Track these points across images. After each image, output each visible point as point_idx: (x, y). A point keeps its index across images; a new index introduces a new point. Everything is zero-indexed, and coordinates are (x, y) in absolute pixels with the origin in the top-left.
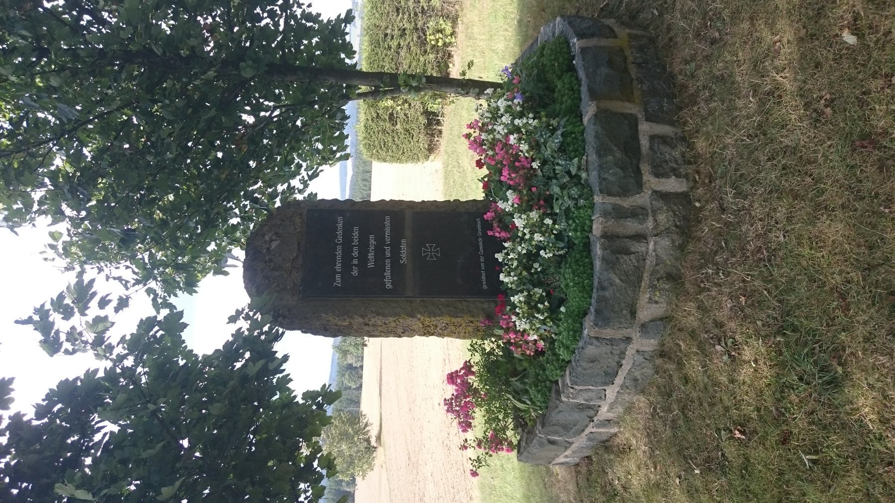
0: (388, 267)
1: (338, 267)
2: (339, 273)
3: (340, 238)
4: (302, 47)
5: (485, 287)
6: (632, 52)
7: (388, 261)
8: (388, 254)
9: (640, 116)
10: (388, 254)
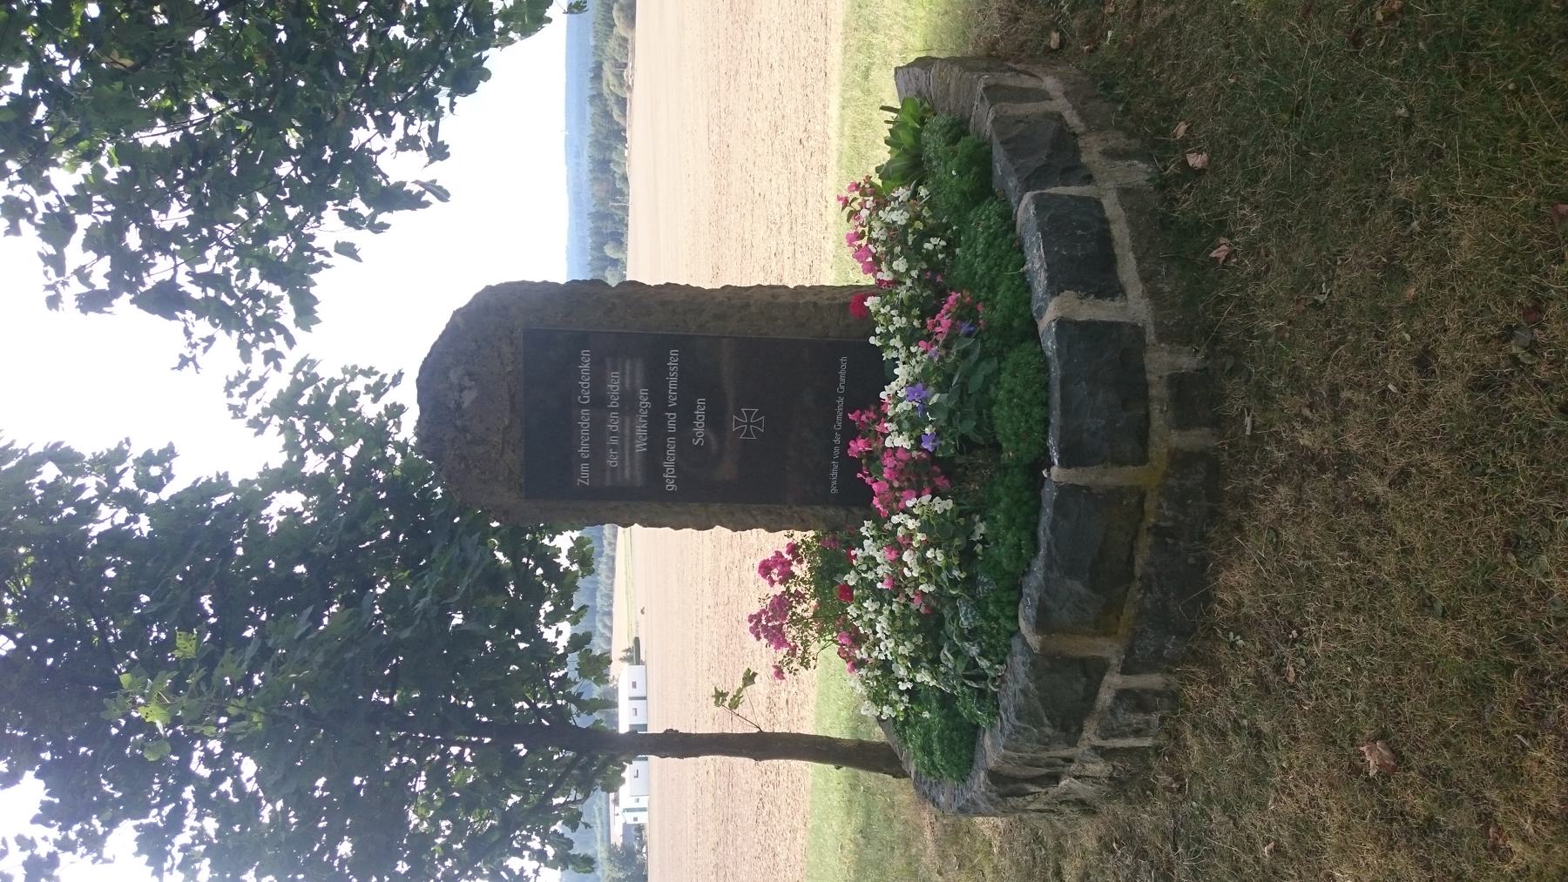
0: (671, 449)
1: (584, 450)
2: (586, 461)
3: (587, 395)
4: (214, 795)
5: (834, 490)
6: (1160, 506)
7: (671, 441)
8: (672, 427)
9: (1114, 661)
10: (672, 427)
